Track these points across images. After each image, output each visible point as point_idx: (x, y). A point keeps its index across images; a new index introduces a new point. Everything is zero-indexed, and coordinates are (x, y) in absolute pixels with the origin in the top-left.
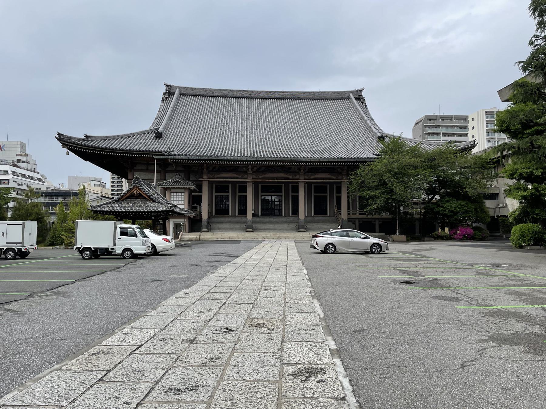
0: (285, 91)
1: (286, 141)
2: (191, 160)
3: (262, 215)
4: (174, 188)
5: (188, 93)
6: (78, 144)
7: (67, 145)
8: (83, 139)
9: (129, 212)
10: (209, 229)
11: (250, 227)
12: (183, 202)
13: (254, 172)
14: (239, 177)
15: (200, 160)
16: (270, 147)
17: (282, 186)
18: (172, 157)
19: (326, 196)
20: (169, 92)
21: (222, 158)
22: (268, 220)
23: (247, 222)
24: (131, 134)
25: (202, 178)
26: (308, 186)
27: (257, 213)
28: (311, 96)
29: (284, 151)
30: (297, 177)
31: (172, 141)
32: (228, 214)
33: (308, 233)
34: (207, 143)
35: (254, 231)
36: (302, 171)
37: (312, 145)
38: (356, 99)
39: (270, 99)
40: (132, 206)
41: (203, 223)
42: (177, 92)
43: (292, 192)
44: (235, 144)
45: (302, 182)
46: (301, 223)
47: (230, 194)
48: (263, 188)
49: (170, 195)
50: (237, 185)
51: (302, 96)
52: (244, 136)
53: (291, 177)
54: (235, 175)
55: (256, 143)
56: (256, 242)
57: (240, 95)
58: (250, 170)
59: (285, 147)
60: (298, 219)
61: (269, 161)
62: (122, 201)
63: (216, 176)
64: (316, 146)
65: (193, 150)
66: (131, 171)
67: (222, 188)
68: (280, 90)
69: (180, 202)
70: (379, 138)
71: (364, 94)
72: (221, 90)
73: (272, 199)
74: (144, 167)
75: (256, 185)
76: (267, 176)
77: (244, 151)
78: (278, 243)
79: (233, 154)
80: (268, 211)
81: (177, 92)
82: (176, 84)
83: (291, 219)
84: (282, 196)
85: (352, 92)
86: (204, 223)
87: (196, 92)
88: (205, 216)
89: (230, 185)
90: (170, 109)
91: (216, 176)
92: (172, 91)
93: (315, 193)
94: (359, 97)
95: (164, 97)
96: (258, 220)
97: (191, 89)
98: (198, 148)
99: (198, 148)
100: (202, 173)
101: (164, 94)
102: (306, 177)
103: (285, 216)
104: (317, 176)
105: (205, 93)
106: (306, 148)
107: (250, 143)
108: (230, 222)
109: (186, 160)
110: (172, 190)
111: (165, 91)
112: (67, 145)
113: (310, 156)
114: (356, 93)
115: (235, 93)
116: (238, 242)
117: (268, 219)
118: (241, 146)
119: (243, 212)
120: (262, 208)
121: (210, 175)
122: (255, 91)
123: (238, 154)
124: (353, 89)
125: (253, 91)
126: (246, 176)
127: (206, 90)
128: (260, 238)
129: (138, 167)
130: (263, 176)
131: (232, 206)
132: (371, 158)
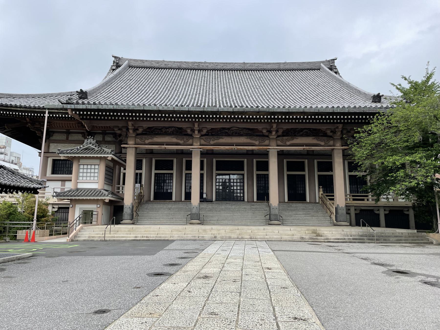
0: (246, 62)
4: (86, 158)
10: (134, 219)
11: (196, 218)
12: (96, 178)
13: (202, 135)
17: (243, 162)
18: (73, 107)
19: (304, 176)
25: (127, 144)
26: (281, 155)
27: (209, 198)
30: (267, 142)
32: (171, 199)
36: (274, 133)
39: (230, 70)
41: (125, 210)
45: (273, 150)
47: (174, 172)
49: (79, 169)
51: (265, 67)
53: (257, 143)
54: (174, 140)
58: (196, 132)
60: (269, 206)
63: (147, 142)
67: (164, 163)
69: (88, 178)
71: (336, 63)
72: (174, 62)
73: (230, 179)
74: (64, 137)
76: (222, 141)
84: (243, 175)
86: (127, 211)
87: (146, 64)
88: (128, 200)
92: (120, 63)
93: (288, 170)
94: (332, 67)
100: (127, 136)
102: (279, 143)
103: (248, 202)
104: (296, 141)
105: (157, 65)
108: (170, 209)
110: (82, 161)
115: (190, 65)
116: (163, 243)
117: (224, 205)
121: (138, 140)
122: (213, 63)
125: (210, 63)
126: (190, 141)
127: (158, 62)
128: (207, 236)
130: (216, 141)
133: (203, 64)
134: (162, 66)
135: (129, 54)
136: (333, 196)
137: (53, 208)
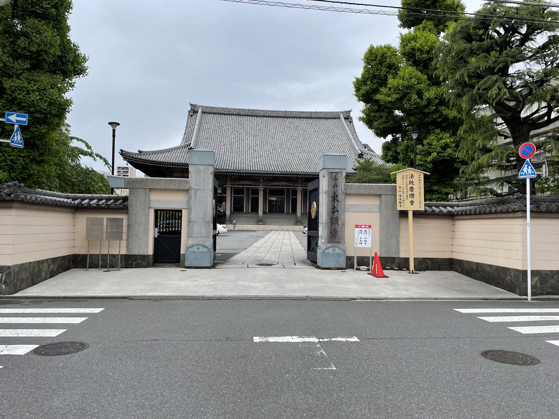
3: (269, 212)
5: (209, 112)
6: (135, 158)
7: (127, 159)
8: (137, 154)
11: (260, 221)
14: (254, 184)
20: (194, 111)
22: (273, 216)
23: (258, 217)
24: (170, 149)
28: (309, 116)
30: (296, 185)
32: (243, 211)
35: (264, 224)
38: (345, 118)
42: (200, 110)
43: (292, 195)
46: (298, 219)
48: (270, 192)
51: (301, 115)
54: (250, 183)
56: (268, 232)
57: (251, 114)
60: (296, 216)
61: (276, 174)
66: (66, 144)
68: (284, 110)
70: (359, 155)
72: (235, 109)
74: (180, 174)
76: (274, 184)
78: (282, 232)
80: (275, 209)
81: (200, 110)
82: (199, 104)
83: (291, 216)
85: (342, 112)
86: (228, 218)
87: (215, 111)
88: (228, 213)
90: (196, 127)
91: (237, 184)
92: (196, 110)
95: (189, 114)
96: (266, 216)
97: (212, 108)
103: (286, 213)
105: (223, 112)
108: (246, 217)
112: (127, 159)
114: (345, 113)
117: (274, 215)
122: (263, 111)
124: (343, 110)
126: (258, 184)
127: (223, 109)
129: (175, 174)
131: (247, 206)
132: (352, 173)
135: (202, 102)
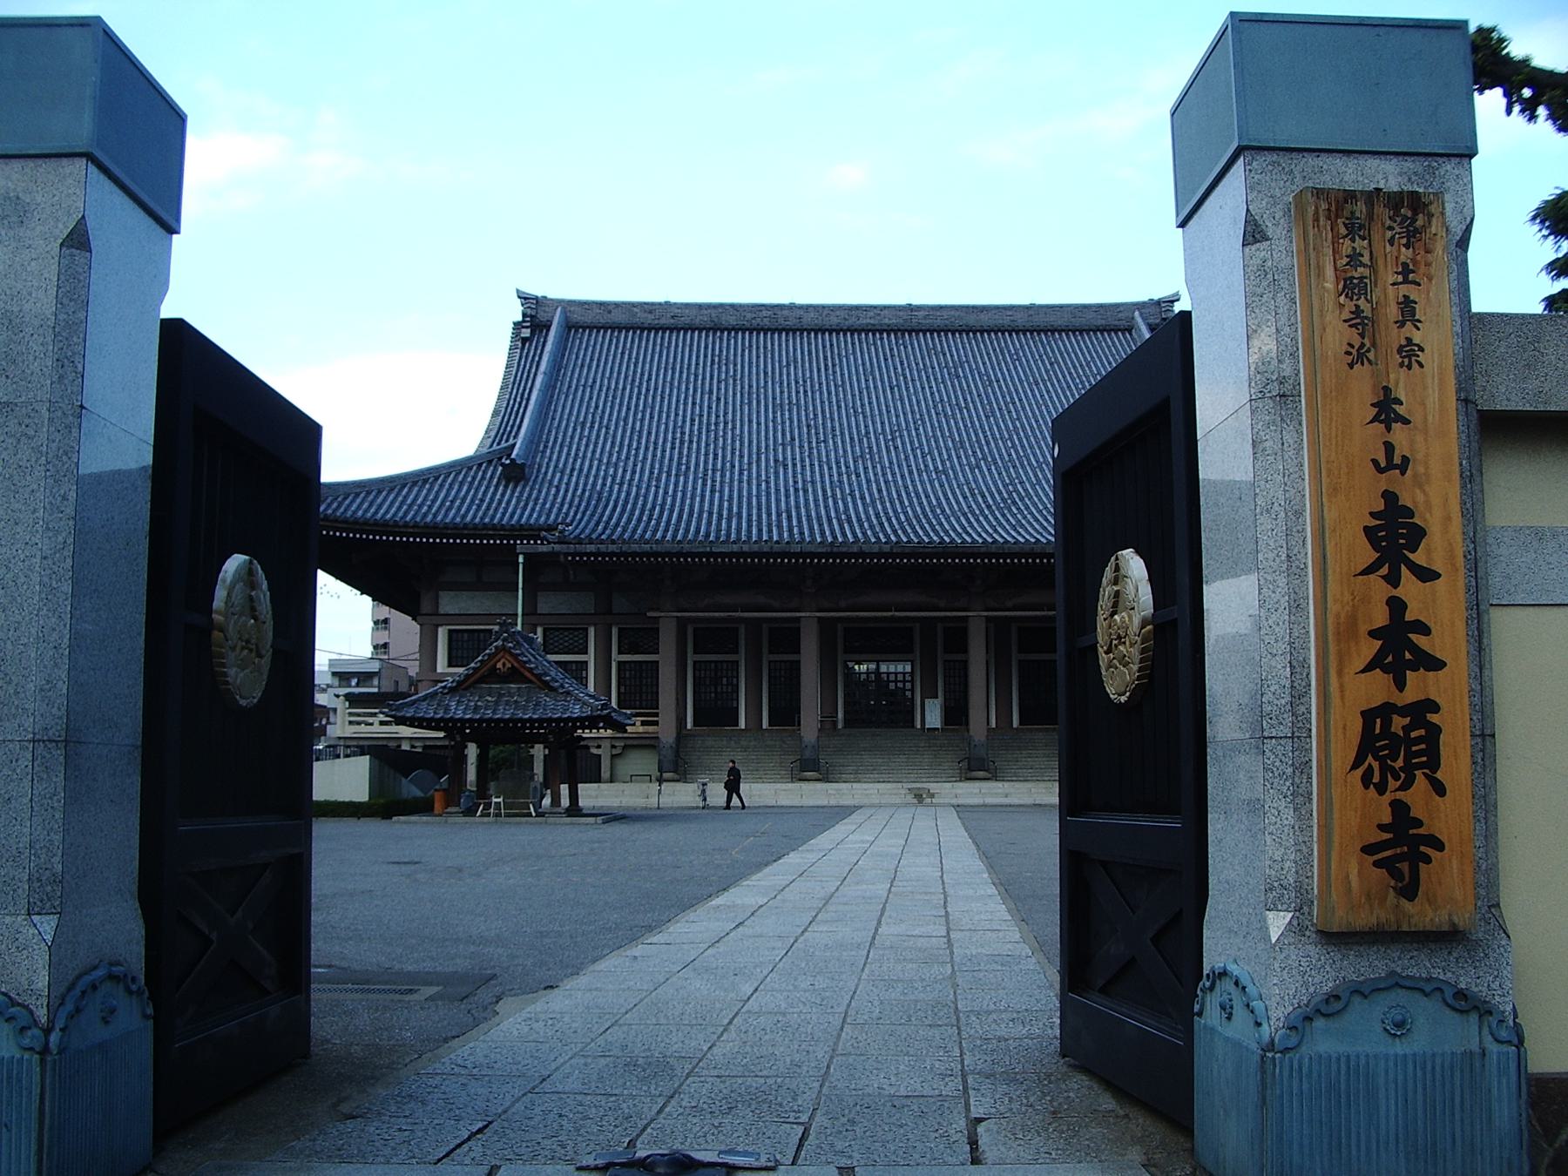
0: (915, 302)
1: (922, 482)
2: (626, 555)
9: (490, 720)
11: (809, 767)
15: (656, 554)
16: (873, 502)
21: (635, 547)
25: (658, 610)
26: (998, 632)
29: (917, 517)
31: (558, 488)
33: (1000, 784)
34: (666, 493)
35: (825, 779)
37: (1009, 494)
39: (867, 332)
40: (497, 703)
44: (758, 496)
45: (977, 619)
47: (590, 658)
50: (940, 626)
52: (785, 466)
55: (824, 491)
59: (921, 504)
62: (466, 689)
64: (1022, 499)
65: (629, 520)
67: (712, 638)
75: (826, 629)
77: (789, 518)
79: (659, 535)
89: (742, 630)
92: (542, 316)
98: (642, 513)
99: (642, 513)
101: (518, 326)
106: (989, 507)
107: (805, 491)
109: (612, 554)
111: (520, 318)
113: (1005, 535)
115: (749, 316)
118: (778, 501)
119: (786, 714)
120: (845, 702)
123: (645, 532)
133: (785, 312)
134: (663, 321)
136: (656, 715)
137: (613, 747)
